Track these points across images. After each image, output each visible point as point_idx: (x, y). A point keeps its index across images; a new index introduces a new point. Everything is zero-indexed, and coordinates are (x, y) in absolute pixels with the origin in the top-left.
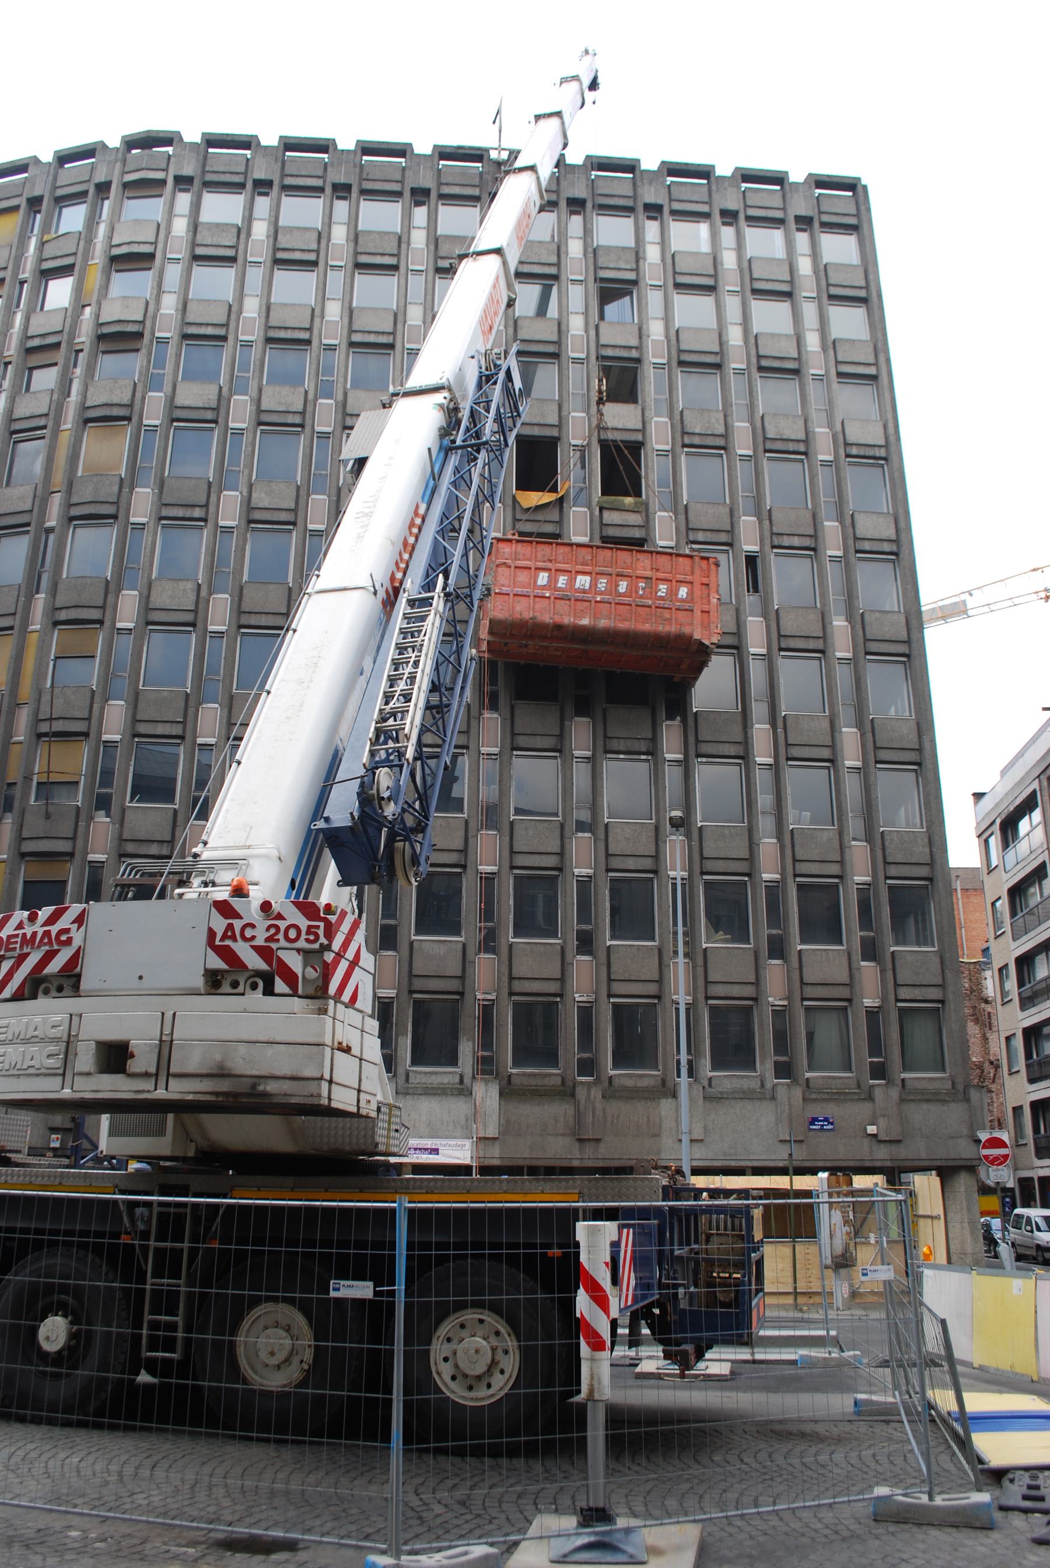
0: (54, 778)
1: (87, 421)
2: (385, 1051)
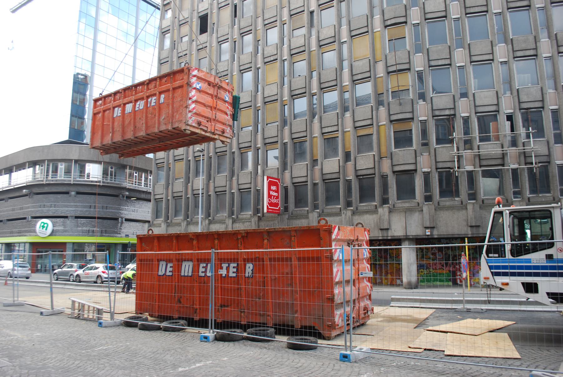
2: (386, 196)
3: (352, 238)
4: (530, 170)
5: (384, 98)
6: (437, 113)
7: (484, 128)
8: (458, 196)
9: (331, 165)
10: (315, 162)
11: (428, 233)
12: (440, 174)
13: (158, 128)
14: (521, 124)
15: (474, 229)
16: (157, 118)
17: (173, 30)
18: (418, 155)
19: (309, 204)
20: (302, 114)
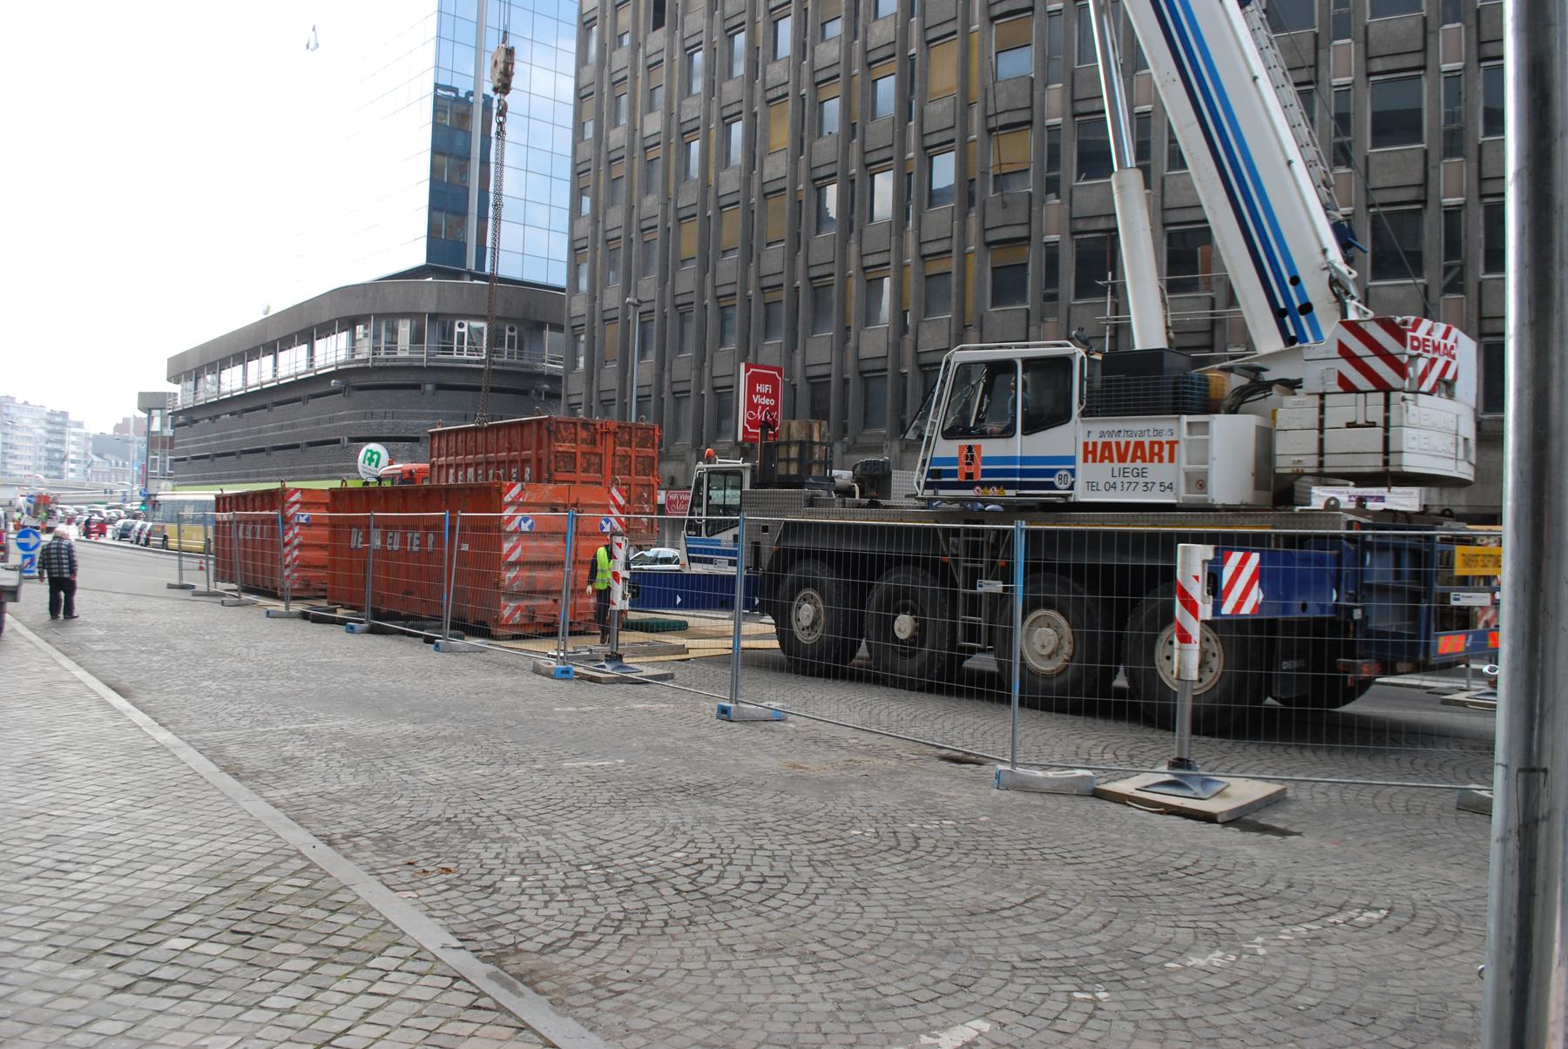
0: (1006, 169)
6: (1080, 225)
17: (604, 17)
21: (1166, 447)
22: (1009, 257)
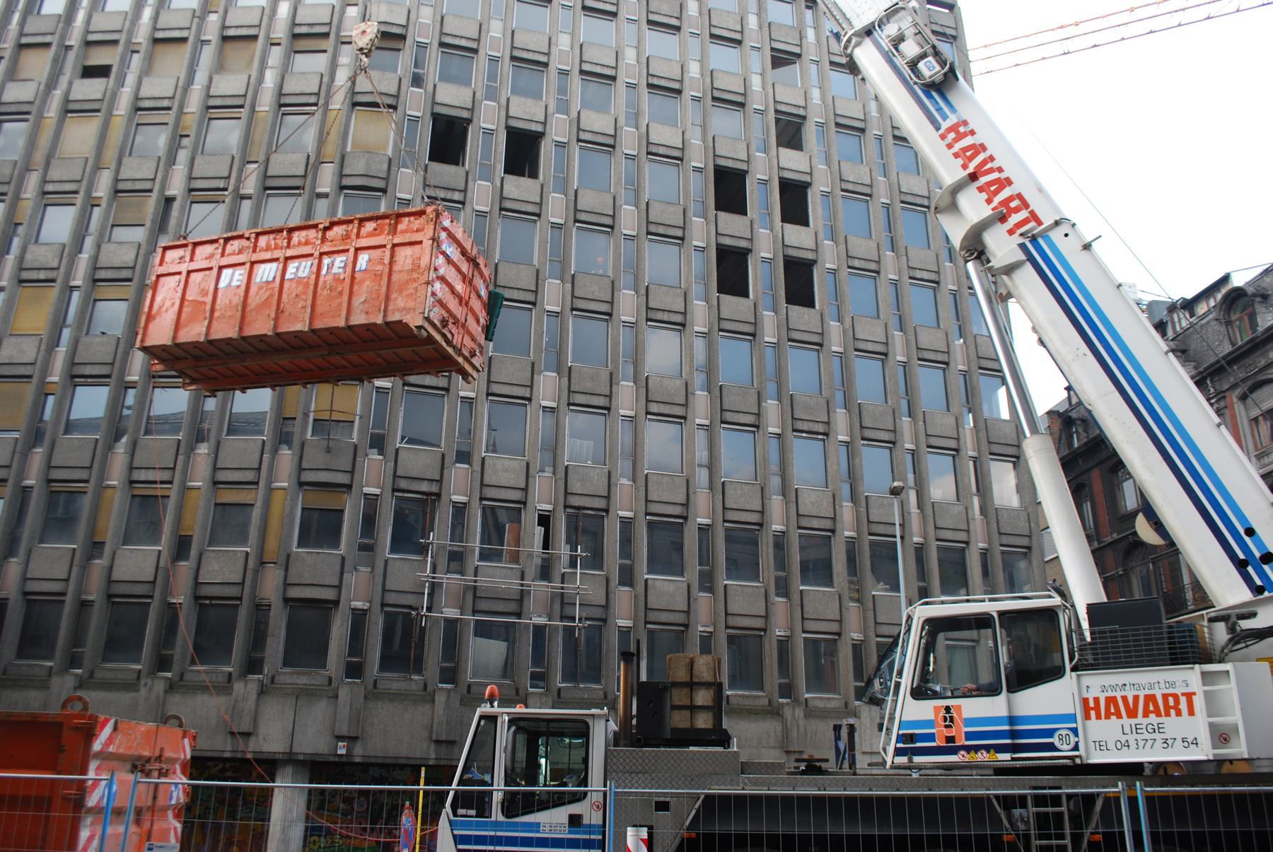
1: (355, 104)
2: (258, 655)
3: (147, 753)
4: (569, 631)
5: (296, 428)
6: (403, 484)
7: (494, 530)
8: (419, 670)
9: (137, 562)
10: (95, 547)
11: (342, 751)
12: (390, 620)
13: (347, 319)
14: (564, 537)
15: (443, 748)
16: (346, 298)
18: (346, 568)
19: (59, 653)
20: (88, 425)
21: (1183, 700)
22: (325, 501)
